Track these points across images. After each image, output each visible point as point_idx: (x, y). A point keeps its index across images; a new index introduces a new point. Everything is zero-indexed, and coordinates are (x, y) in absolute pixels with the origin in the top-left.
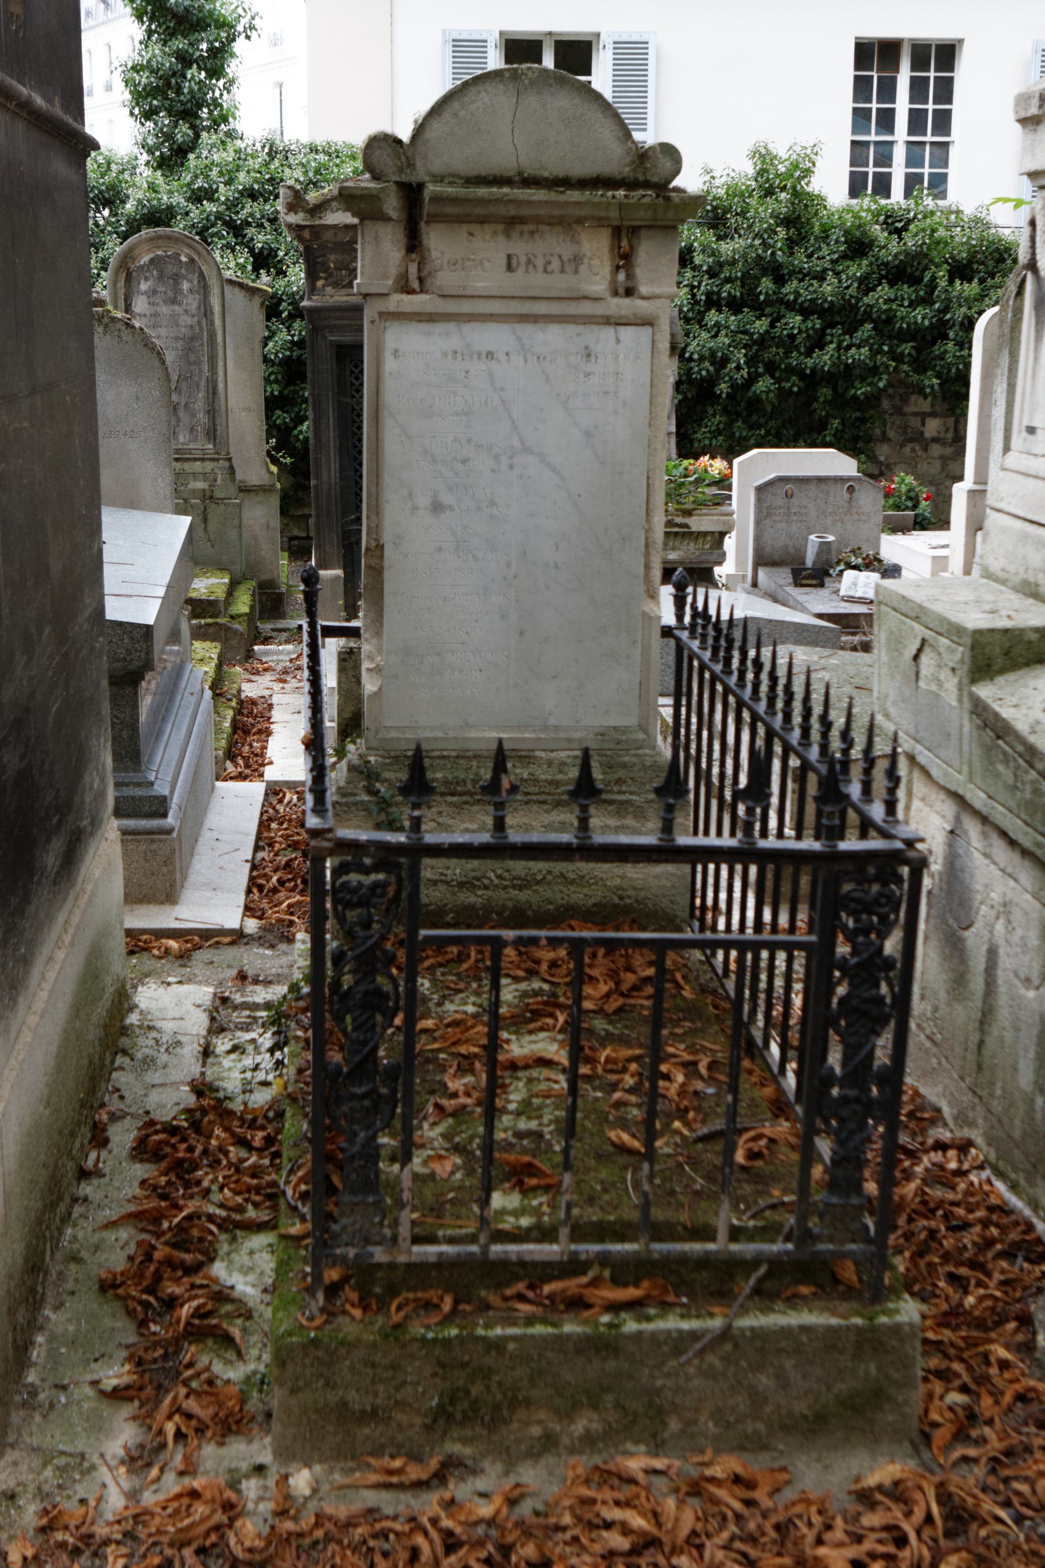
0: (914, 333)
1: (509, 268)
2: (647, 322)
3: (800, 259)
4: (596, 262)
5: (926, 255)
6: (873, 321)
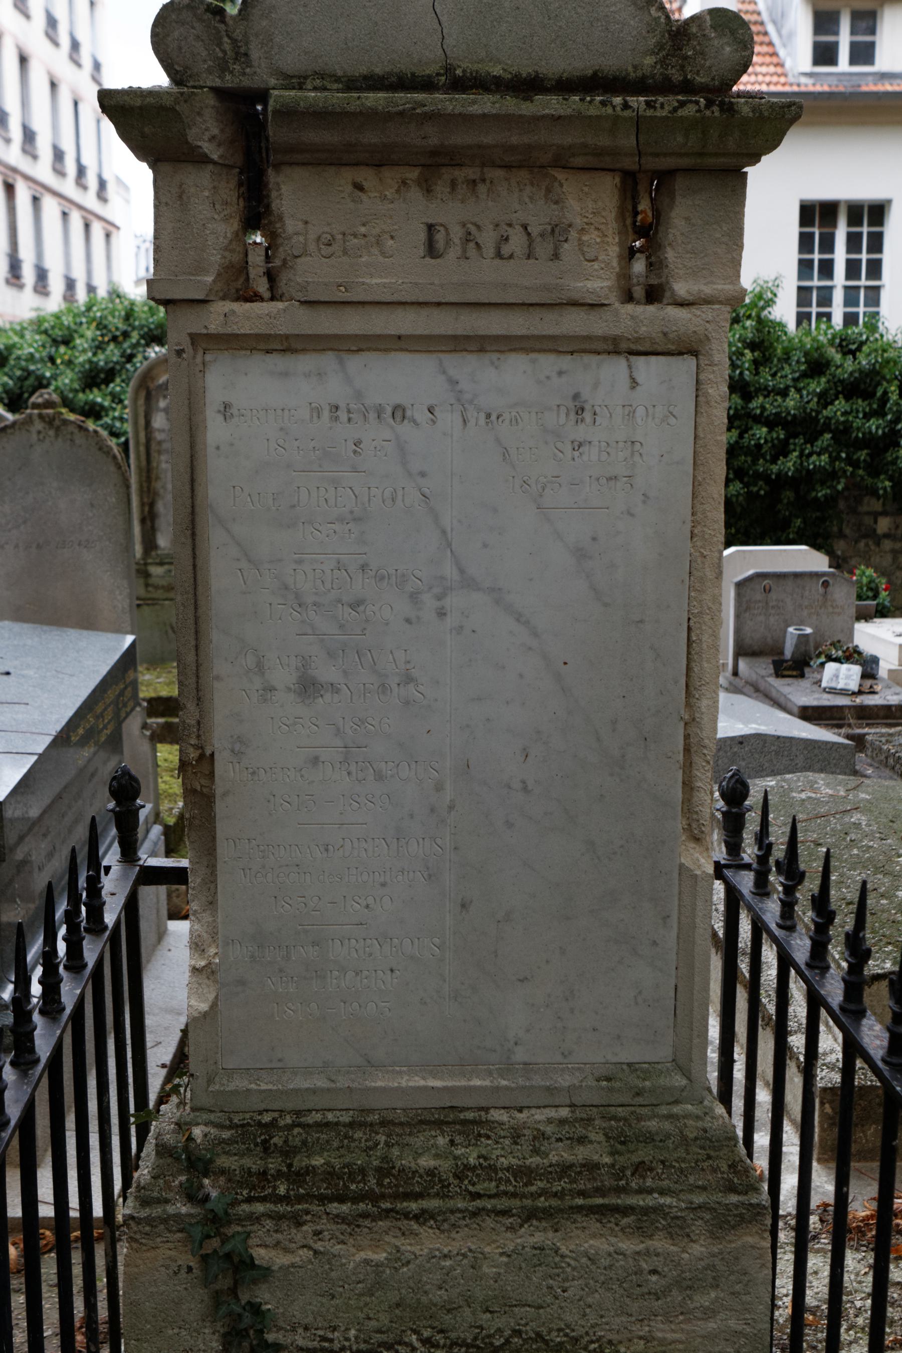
0: (869, 441)
1: (432, 250)
2: (688, 348)
3: (765, 377)
4: (592, 237)
5: (878, 373)
6: (830, 431)
